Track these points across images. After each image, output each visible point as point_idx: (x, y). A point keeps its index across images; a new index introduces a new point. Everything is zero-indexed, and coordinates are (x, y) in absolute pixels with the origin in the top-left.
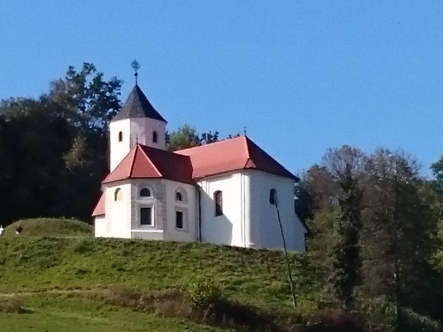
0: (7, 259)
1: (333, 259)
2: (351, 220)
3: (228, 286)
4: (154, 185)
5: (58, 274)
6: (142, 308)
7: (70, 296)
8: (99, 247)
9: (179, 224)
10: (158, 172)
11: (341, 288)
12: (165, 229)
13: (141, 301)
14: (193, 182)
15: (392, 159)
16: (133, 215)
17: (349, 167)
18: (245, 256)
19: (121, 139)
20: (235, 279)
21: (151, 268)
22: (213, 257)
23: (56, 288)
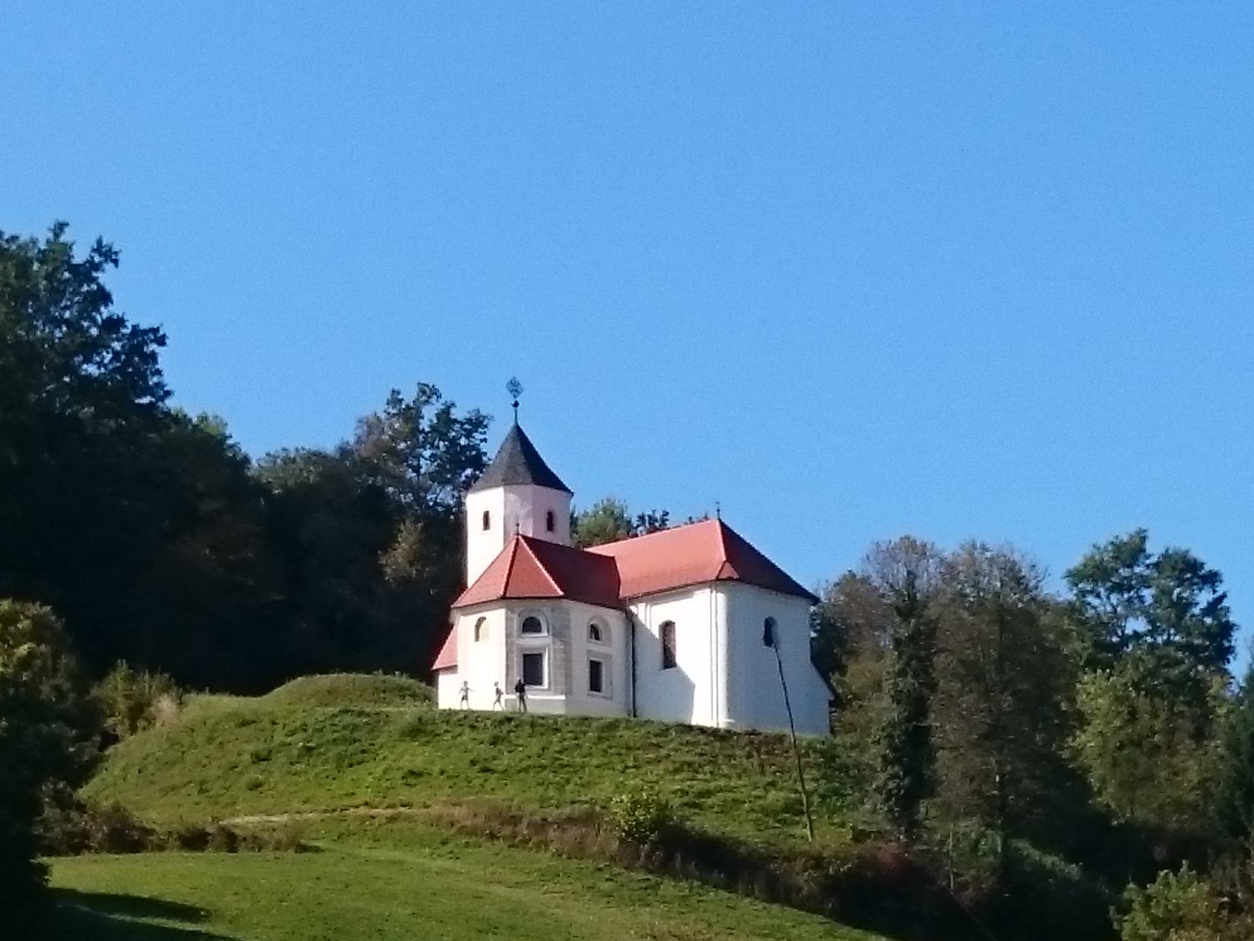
0: (274, 751)
1: (883, 749)
2: (915, 676)
3: (686, 799)
5: (370, 779)
7: (392, 819)
8: (445, 727)
9: (595, 685)
10: (556, 587)
11: (896, 804)
12: (568, 693)
13: (523, 830)
14: (621, 605)
15: (991, 561)
19: (486, 524)
20: (699, 786)
21: (544, 767)
22: (658, 746)
23: (366, 804)
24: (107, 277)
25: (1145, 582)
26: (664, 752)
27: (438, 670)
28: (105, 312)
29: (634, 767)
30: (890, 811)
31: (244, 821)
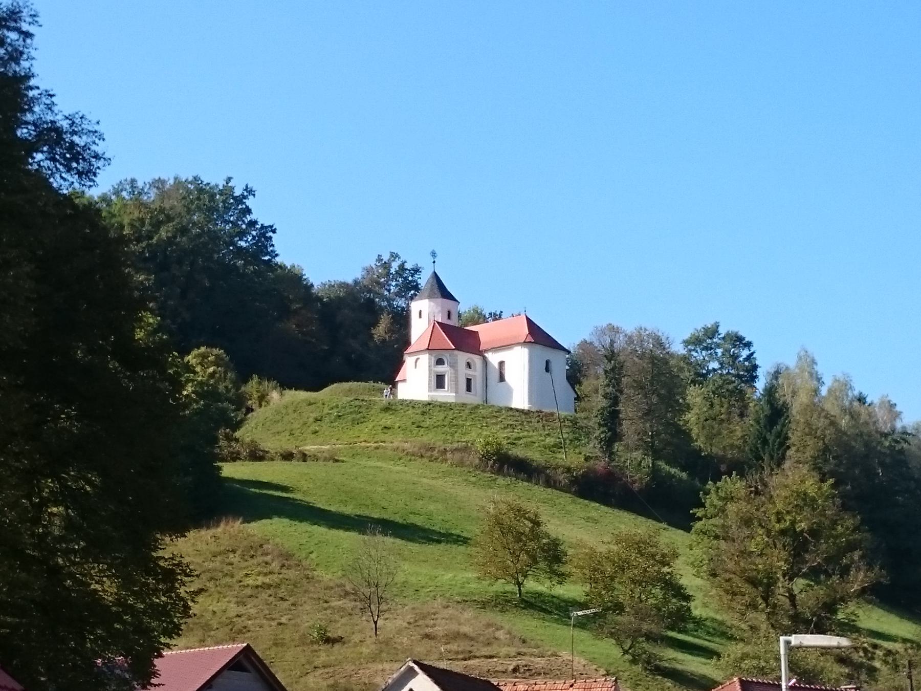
2: (614, 387)
3: (509, 441)
4: (447, 355)
5: (367, 430)
6: (436, 459)
7: (377, 448)
8: (401, 407)
9: (469, 389)
12: (456, 392)
13: (435, 453)
14: (480, 353)
16: (430, 380)
17: (612, 342)
18: (523, 416)
20: (515, 435)
21: (445, 426)
23: (365, 441)
24: (250, 202)
25: (718, 346)
26: (499, 420)
27: (397, 382)
28: (249, 218)
29: (486, 426)
30: (601, 447)
31: (310, 448)
